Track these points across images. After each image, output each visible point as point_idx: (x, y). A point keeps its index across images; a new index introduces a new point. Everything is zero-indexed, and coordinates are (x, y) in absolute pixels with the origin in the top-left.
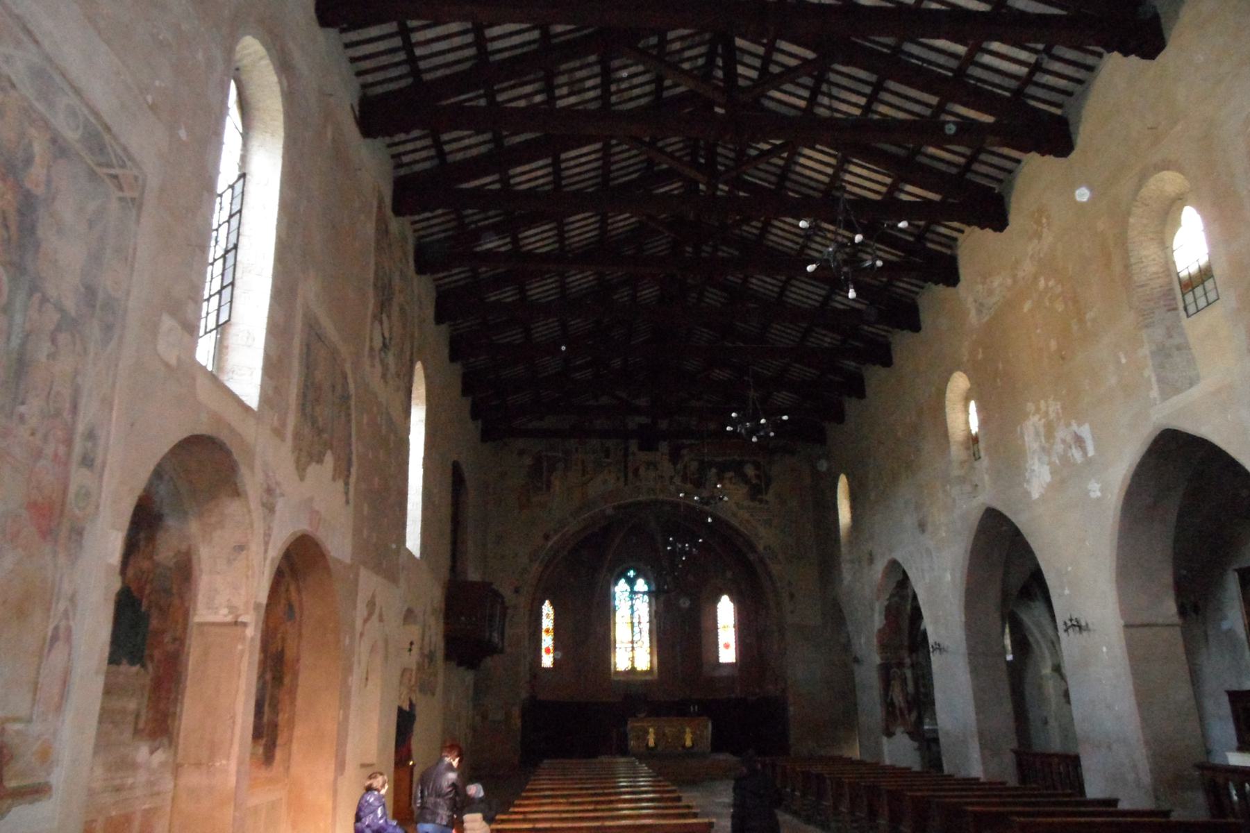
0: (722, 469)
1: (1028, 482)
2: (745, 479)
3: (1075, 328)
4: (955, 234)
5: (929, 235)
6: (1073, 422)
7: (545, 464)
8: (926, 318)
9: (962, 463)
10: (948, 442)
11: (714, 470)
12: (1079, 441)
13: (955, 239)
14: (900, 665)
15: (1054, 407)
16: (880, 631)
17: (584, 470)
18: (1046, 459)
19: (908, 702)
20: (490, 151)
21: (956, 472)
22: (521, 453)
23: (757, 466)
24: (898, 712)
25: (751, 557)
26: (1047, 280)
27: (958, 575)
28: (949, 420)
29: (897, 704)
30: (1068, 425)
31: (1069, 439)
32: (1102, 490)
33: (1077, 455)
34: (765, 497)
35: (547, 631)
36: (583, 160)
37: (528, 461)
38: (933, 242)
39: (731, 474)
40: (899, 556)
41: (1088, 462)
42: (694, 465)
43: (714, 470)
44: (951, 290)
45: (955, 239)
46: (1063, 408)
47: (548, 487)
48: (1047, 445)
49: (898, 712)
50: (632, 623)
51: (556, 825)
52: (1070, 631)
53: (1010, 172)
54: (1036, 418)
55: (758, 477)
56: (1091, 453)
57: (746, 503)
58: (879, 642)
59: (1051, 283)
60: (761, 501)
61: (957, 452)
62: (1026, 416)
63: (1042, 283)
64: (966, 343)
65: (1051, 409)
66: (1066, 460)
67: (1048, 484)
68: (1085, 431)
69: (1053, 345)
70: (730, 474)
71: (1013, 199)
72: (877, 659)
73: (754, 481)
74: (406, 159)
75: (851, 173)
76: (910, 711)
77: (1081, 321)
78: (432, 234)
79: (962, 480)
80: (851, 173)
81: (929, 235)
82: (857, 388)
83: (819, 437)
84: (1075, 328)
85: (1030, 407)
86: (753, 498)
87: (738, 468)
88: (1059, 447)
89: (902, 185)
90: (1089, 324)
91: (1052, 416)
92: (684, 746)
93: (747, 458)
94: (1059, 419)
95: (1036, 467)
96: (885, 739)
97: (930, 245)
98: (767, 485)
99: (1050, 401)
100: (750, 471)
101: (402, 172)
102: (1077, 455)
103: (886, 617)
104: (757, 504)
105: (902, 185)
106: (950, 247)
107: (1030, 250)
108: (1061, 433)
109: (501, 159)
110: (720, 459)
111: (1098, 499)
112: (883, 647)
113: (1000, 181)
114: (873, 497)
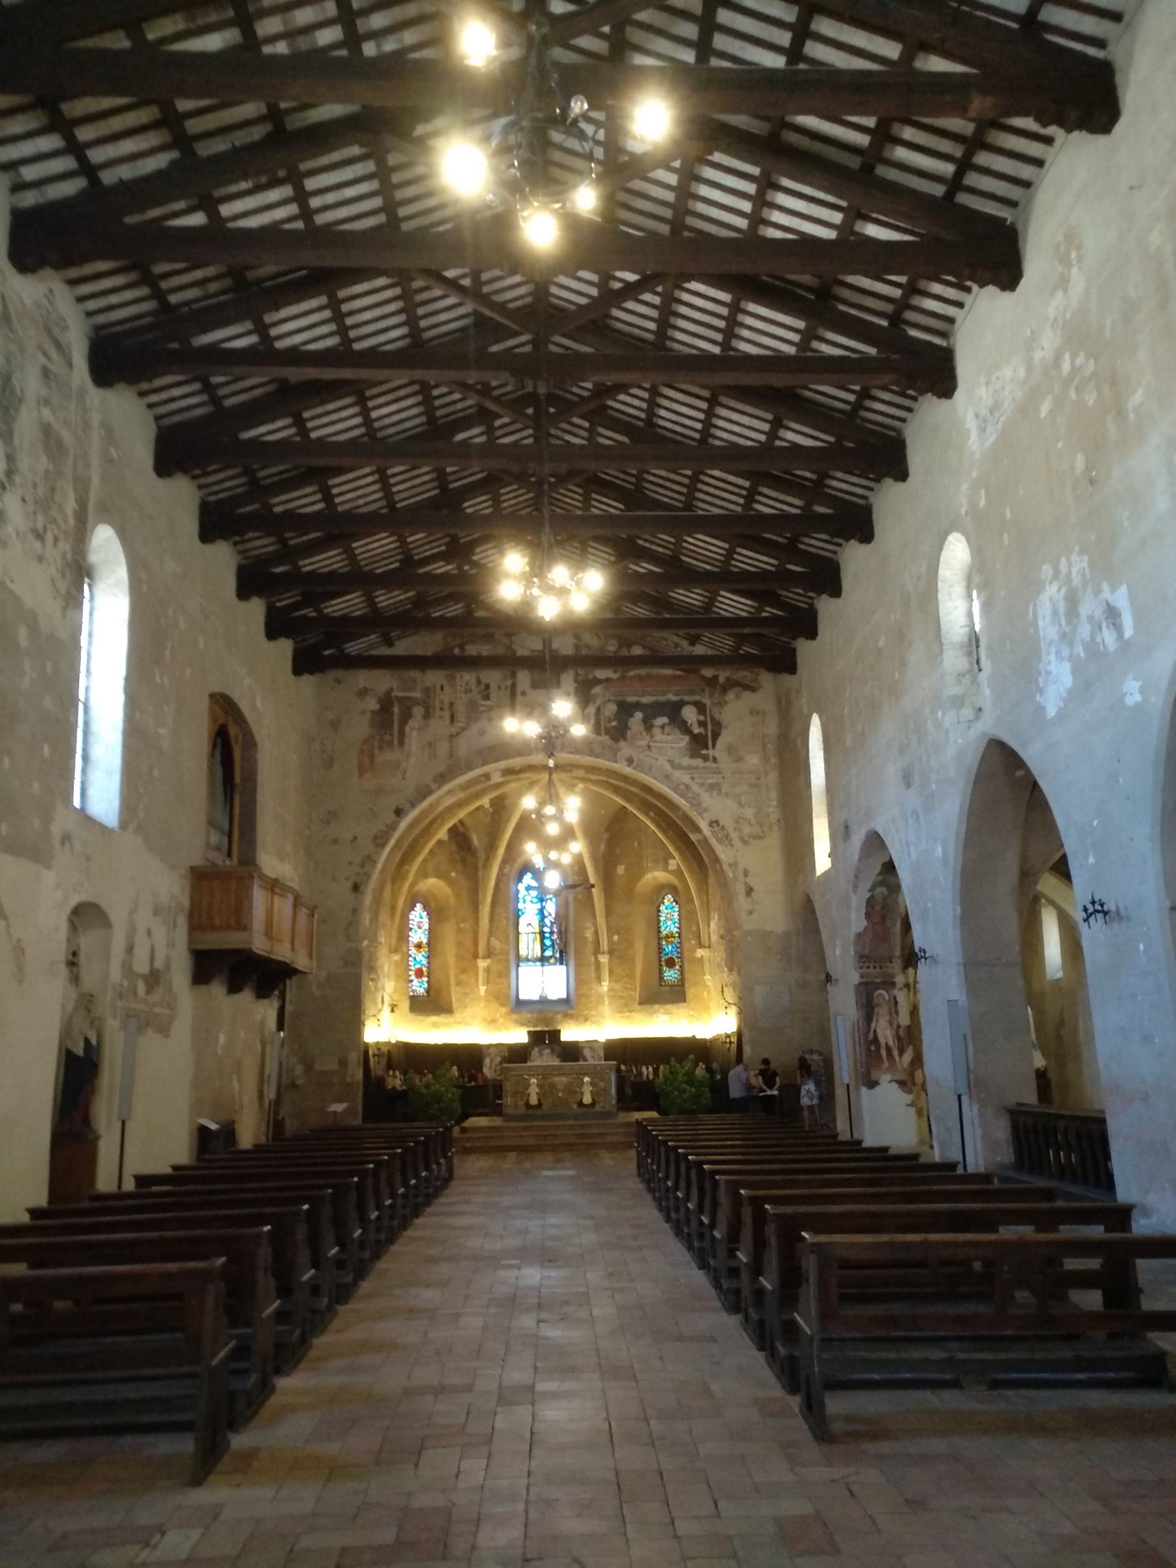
0: (651, 712)
1: (1041, 691)
2: (685, 728)
3: (1112, 427)
4: (950, 311)
5: (910, 316)
6: (1105, 586)
7: (396, 710)
8: (915, 459)
9: (960, 676)
10: (941, 644)
11: (639, 715)
12: (1112, 613)
13: (951, 320)
14: (889, 984)
15: (1077, 565)
16: (859, 936)
17: (452, 717)
18: (1066, 652)
19: (898, 1037)
20: (173, 164)
21: (953, 690)
22: (363, 693)
23: (701, 707)
24: (884, 1053)
25: (694, 837)
26: (1074, 356)
27: (952, 846)
28: (942, 612)
29: (882, 1041)
30: (1097, 592)
31: (1099, 613)
32: (1141, 692)
33: (1108, 637)
34: (711, 752)
35: (419, 946)
36: (349, 192)
37: (372, 704)
38: (917, 326)
39: (665, 720)
40: (879, 825)
41: (1125, 646)
42: (611, 709)
43: (639, 715)
44: (944, 404)
45: (951, 320)
46: (1092, 565)
47: (402, 743)
48: (1068, 629)
49: (884, 1053)
50: (542, 933)
51: (874, 1208)
52: (1092, 919)
53: (1027, 184)
54: (1055, 587)
55: (702, 724)
56: (1128, 632)
57: (686, 761)
58: (856, 952)
59: (1080, 360)
60: (706, 758)
61: (954, 660)
62: (1040, 586)
63: (1066, 366)
64: (965, 486)
65: (1074, 570)
66: (1094, 650)
67: (1069, 692)
68: (1121, 599)
69: (1080, 463)
70: (662, 720)
71: (1031, 231)
72: (855, 978)
73: (696, 731)
74: (29, 173)
75: (781, 209)
76: (901, 1052)
77: (1121, 414)
78: (111, 308)
79: (958, 702)
80: (781, 209)
81: (910, 316)
82: (829, 579)
83: (785, 663)
84: (1112, 427)
85: (1047, 570)
86: (694, 754)
87: (673, 711)
88: (1085, 630)
89: (923, 284)
90: (1132, 416)
91: (1076, 581)
92: (581, 1104)
93: (686, 698)
94: (1085, 583)
95: (1052, 667)
96: (864, 1090)
97: (913, 333)
98: (716, 736)
99: (1074, 558)
100: (690, 714)
101: (29, 199)
102: (1108, 637)
103: (868, 915)
104: (699, 762)
105: (923, 284)
106: (944, 335)
107: (1051, 312)
108: (1089, 607)
109: (197, 176)
110: (646, 700)
111: (1137, 705)
112: (864, 958)
113: (1013, 204)
114: (849, 741)
